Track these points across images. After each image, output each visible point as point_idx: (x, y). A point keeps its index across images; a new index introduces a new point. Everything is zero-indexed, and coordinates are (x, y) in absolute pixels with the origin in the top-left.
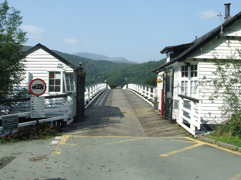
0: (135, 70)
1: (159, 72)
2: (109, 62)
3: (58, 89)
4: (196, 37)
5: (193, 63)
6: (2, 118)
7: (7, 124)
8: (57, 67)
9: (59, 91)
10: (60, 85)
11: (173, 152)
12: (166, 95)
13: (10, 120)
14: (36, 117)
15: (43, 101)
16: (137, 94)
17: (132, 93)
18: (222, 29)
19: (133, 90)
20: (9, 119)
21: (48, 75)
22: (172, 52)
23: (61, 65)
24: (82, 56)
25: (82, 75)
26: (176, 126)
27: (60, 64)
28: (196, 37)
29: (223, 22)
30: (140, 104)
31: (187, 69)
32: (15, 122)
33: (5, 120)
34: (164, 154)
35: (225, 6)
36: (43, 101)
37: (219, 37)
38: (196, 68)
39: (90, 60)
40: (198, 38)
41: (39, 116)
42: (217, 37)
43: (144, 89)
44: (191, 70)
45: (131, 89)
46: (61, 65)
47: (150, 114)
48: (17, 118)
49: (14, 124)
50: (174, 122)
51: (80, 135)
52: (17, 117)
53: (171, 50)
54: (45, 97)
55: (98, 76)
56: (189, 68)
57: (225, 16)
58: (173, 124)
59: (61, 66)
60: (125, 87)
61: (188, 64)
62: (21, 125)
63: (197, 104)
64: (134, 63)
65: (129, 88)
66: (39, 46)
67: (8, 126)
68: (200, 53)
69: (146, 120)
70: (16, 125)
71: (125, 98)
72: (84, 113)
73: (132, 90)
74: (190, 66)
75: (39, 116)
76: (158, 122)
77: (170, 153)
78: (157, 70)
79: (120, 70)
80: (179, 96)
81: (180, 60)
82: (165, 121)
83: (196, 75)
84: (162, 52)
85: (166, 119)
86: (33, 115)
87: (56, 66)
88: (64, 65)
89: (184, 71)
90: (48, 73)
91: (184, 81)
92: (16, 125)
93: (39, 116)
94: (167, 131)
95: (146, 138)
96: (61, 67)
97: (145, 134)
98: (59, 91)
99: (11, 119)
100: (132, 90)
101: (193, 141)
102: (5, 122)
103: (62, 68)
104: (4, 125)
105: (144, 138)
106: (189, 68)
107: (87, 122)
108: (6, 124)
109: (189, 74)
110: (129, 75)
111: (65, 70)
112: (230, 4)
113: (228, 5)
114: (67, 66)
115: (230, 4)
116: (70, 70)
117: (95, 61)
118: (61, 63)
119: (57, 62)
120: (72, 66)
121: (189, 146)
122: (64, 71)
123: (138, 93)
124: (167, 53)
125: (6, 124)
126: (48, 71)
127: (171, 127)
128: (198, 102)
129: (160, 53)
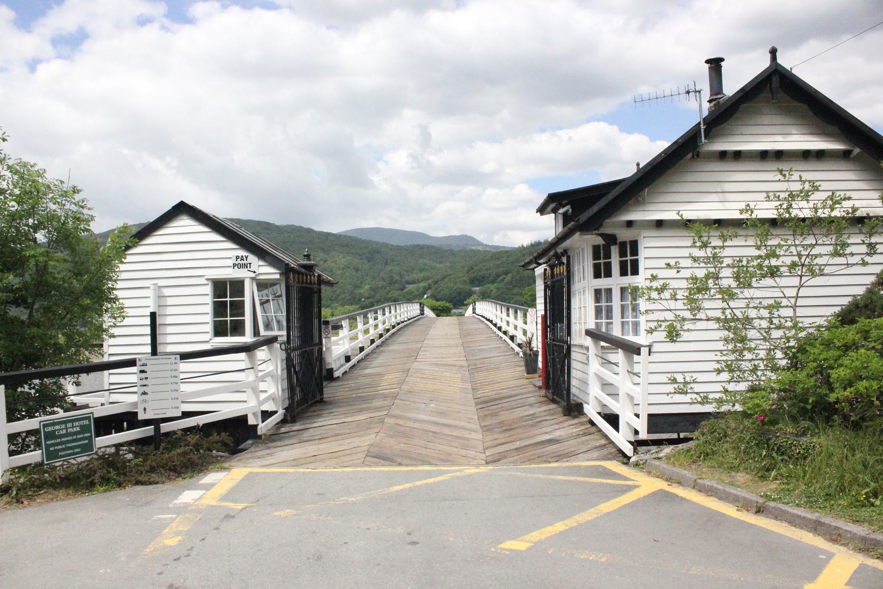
0: (498, 266)
1: (535, 268)
2: (432, 247)
3: (238, 328)
4: (638, 165)
5: (624, 235)
6: (38, 424)
7: (58, 440)
8: (232, 265)
9: (242, 334)
10: (244, 316)
11: (549, 528)
12: (553, 330)
13: (67, 429)
14: (154, 414)
15: (174, 367)
16: (494, 328)
17: (482, 326)
18: (702, 131)
19: (486, 319)
20: (63, 426)
21: (208, 289)
22: (568, 208)
23: (243, 260)
24: (364, 237)
25: (304, 285)
26: (582, 424)
27: (242, 256)
28: (638, 165)
29: (705, 113)
30: (494, 357)
31: (608, 255)
32: (84, 434)
33: (50, 429)
34: (514, 538)
35: (707, 66)
36: (174, 367)
37: (697, 156)
38: (635, 251)
39: (385, 245)
40: (641, 166)
41: (165, 413)
42: (690, 155)
43: (508, 315)
44: (621, 256)
45: (482, 316)
46: (243, 260)
47: (513, 387)
48: (90, 421)
49: (80, 439)
50: (574, 410)
51: (283, 463)
52: (88, 418)
53: (564, 202)
54: (178, 357)
55: (407, 285)
56: (615, 251)
57: (711, 95)
58: (575, 417)
59: (245, 262)
60: (469, 312)
61: (611, 239)
62: (105, 442)
63: (636, 358)
64: (498, 247)
65: (477, 311)
66: (182, 209)
67: (60, 447)
68: (641, 203)
69: (499, 406)
70: (87, 441)
71: (460, 341)
72: (324, 393)
73: (484, 317)
74: (615, 244)
75: (165, 413)
76: (531, 412)
77: (537, 536)
78: (530, 263)
79: (463, 267)
80: (588, 333)
81: (585, 228)
82: (553, 406)
83: (635, 272)
84: (542, 210)
85: (554, 401)
86: (145, 409)
87: (230, 263)
88: (252, 259)
89: (602, 261)
90: (210, 283)
91: (603, 287)
92: (87, 441)
93: (163, 411)
94: (551, 442)
95: (483, 469)
96: (245, 266)
97: (483, 456)
98: (242, 334)
99: (69, 425)
100: (484, 317)
101: (626, 479)
102: (50, 436)
103: (249, 269)
104: (47, 447)
105: (477, 470)
106: (615, 251)
107: (320, 420)
108: (52, 442)
109: (616, 269)
110: (484, 278)
111: (254, 272)
112: (722, 60)
113: (715, 64)
114: (261, 263)
115: (722, 60)
116: (269, 272)
117: (398, 248)
118: (242, 253)
119: (231, 251)
120: (273, 261)
121: (608, 499)
122: (253, 275)
123: (495, 325)
124: (554, 211)
125: (52, 442)
126: (207, 279)
127: (565, 428)
128: (639, 354)
129: (537, 212)
